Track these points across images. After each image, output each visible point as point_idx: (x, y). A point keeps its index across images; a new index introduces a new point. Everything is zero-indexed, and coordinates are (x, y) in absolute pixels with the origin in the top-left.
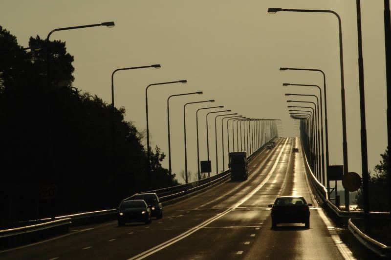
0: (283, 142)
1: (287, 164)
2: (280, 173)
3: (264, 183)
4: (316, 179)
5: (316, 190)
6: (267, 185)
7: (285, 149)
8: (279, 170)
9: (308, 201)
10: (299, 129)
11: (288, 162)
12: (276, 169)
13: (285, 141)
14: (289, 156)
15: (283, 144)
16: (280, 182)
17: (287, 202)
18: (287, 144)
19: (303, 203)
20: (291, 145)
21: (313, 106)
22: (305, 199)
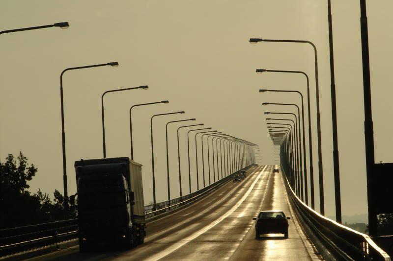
0: (260, 169)
1: (263, 192)
2: (253, 202)
3: (224, 217)
4: (295, 195)
6: (228, 220)
7: (262, 176)
8: (252, 199)
9: (287, 216)
10: (279, 156)
11: (265, 189)
12: (248, 197)
13: (263, 168)
14: (266, 182)
15: (261, 171)
16: (250, 215)
17: (269, 216)
18: (265, 170)
19: (283, 216)
20: (270, 172)
21: (293, 118)
22: (285, 213)
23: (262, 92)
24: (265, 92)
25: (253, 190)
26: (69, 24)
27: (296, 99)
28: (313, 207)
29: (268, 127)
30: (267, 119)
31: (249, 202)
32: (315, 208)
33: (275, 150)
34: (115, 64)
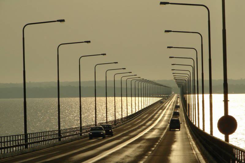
12: (156, 126)
21: (188, 76)
24: (167, 5)
25: (163, 117)
27: (194, 41)
31: (156, 129)
34: (62, 21)
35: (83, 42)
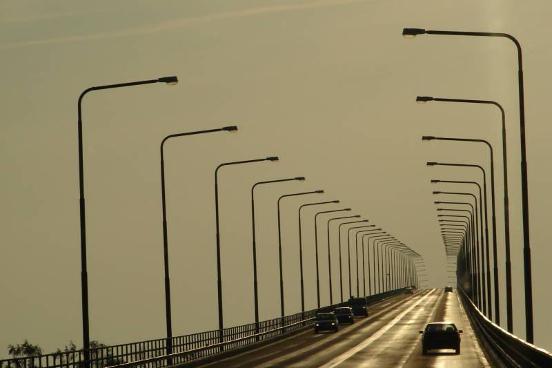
5: (477, 324)
17: (437, 329)
21: (466, 225)
22: (455, 324)
23: (435, 195)
24: (431, 141)
26: (178, 79)
27: (486, 123)
28: (498, 322)
29: (439, 216)
30: (438, 210)
32: (514, 331)
33: (450, 265)
35: (264, 160)
